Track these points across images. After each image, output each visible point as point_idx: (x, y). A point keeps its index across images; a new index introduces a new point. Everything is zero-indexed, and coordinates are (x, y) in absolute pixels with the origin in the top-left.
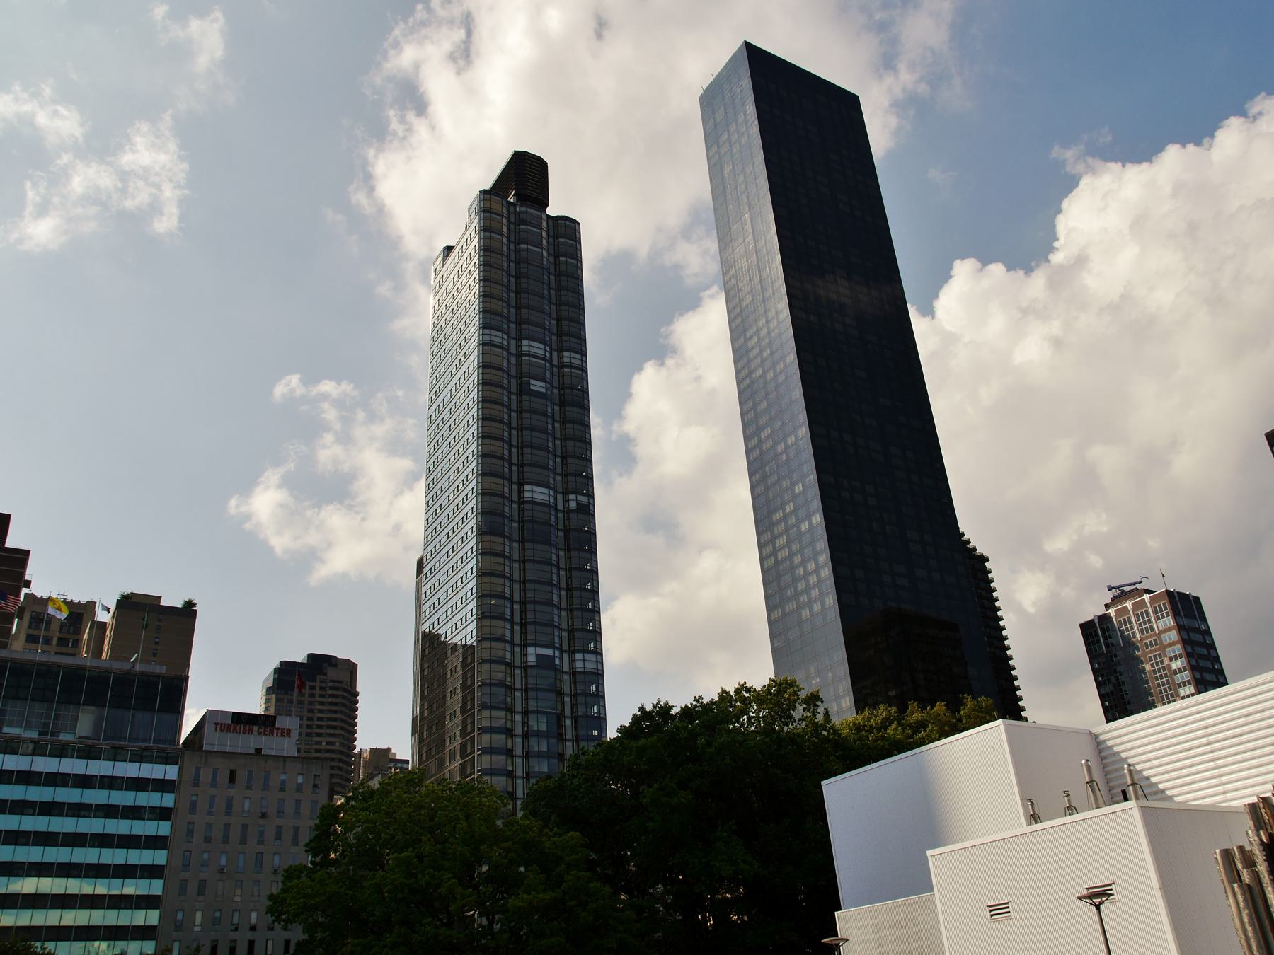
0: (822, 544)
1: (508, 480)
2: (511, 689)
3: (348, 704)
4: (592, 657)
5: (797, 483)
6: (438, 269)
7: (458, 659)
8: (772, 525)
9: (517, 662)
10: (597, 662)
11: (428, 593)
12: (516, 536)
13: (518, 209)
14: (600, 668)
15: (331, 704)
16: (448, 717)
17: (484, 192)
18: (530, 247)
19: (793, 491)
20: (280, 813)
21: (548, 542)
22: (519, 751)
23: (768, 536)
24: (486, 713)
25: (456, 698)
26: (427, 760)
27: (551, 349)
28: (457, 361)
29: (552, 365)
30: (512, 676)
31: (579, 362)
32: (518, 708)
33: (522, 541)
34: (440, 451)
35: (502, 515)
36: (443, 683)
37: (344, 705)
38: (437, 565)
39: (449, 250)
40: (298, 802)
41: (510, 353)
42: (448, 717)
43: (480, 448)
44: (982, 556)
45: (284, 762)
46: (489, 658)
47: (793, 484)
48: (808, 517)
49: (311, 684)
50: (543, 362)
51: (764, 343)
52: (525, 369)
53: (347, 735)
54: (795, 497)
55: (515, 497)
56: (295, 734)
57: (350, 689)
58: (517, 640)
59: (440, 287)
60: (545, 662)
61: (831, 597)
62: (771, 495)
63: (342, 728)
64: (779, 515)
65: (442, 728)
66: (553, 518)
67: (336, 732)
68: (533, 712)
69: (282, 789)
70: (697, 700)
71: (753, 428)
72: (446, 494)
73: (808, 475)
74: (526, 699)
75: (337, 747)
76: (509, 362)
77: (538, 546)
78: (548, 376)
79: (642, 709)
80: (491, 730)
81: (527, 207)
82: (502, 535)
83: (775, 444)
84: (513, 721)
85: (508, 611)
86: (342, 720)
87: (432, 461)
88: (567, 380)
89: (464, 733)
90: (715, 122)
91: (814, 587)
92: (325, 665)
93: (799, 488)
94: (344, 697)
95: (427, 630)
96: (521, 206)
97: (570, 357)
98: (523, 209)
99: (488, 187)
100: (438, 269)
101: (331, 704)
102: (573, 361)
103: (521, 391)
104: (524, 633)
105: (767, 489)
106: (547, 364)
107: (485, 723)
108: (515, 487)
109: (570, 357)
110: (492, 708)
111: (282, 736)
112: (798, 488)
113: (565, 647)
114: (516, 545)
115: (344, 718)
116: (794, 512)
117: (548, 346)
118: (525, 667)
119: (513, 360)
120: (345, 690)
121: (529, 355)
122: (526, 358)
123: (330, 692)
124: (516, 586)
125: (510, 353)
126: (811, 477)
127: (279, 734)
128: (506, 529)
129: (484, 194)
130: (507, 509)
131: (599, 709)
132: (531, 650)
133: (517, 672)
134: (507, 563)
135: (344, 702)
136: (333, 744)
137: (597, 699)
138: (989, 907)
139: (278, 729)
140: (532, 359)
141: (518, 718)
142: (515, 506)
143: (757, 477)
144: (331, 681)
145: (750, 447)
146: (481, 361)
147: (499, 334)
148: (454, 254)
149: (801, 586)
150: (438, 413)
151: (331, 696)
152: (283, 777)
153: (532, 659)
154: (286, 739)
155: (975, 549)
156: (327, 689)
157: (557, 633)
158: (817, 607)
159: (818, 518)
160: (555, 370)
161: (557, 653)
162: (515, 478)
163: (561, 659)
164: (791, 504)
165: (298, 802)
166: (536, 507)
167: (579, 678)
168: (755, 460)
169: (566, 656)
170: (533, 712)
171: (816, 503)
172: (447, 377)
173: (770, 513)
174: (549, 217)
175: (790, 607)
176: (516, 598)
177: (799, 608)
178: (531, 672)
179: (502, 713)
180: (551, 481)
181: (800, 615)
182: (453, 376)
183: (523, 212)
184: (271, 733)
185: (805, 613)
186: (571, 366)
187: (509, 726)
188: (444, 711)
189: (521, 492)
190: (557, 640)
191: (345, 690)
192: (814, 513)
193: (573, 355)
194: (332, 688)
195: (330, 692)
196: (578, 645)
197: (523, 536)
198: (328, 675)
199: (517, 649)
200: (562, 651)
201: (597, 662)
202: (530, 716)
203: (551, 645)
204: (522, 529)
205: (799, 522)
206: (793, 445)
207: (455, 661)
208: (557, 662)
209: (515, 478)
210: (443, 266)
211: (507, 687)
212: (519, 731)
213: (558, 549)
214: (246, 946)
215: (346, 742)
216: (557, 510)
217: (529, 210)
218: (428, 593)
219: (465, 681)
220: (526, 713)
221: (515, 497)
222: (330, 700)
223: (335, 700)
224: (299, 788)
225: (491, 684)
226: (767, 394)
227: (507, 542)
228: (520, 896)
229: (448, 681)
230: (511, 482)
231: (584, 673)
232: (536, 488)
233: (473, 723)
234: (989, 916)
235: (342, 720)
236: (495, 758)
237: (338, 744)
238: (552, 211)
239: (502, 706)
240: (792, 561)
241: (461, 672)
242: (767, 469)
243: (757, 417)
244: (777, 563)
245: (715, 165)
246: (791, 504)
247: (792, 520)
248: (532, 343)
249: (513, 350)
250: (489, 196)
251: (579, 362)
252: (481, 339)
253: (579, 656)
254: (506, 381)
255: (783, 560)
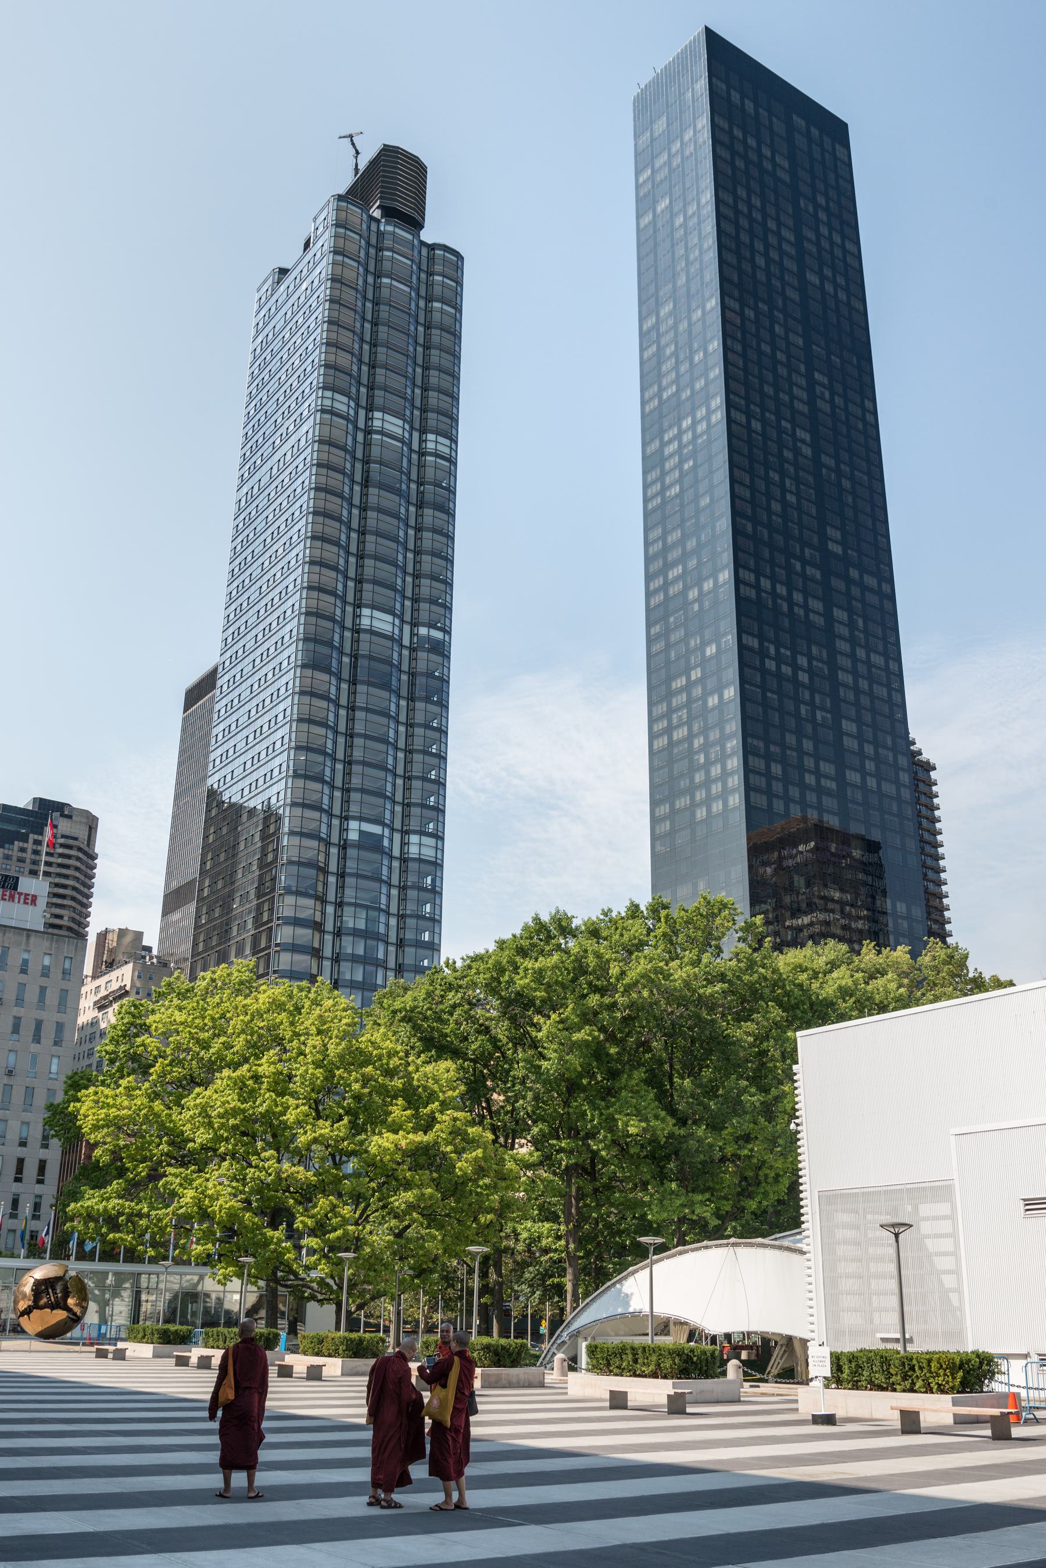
0: (734, 726)
1: (340, 597)
2: (325, 871)
3: (83, 867)
4: (431, 841)
5: (709, 643)
6: (263, 299)
7: (257, 826)
8: (670, 694)
9: (335, 839)
10: (437, 848)
11: (220, 736)
12: (345, 675)
13: (382, 228)
14: (439, 856)
15: (60, 865)
16: (237, 900)
17: (340, 198)
18: (395, 283)
19: (703, 653)
20: (20, 1001)
21: (386, 686)
22: (328, 952)
23: (662, 708)
24: (290, 900)
25: (250, 877)
26: (205, 951)
27: (412, 428)
28: (283, 430)
29: (411, 450)
30: (327, 855)
31: (447, 450)
32: (331, 896)
33: (353, 682)
34: (250, 550)
35: (330, 644)
36: (233, 856)
37: (77, 869)
38: (236, 701)
39: (283, 272)
40: (43, 990)
41: (356, 428)
42: (237, 900)
43: (308, 551)
44: (928, 763)
45: (28, 936)
46: (299, 830)
47: (704, 644)
48: (719, 690)
49: (36, 837)
50: (400, 445)
51: (685, 451)
52: (375, 451)
53: (78, 907)
54: (704, 662)
55: (348, 623)
56: (42, 902)
57: (86, 849)
58: (337, 811)
59: (265, 325)
60: (370, 844)
61: (737, 796)
62: (673, 654)
63: (73, 899)
64: (680, 682)
65: (228, 914)
66: (396, 656)
67: (65, 902)
68: (350, 904)
69: (24, 971)
70: (605, 914)
71: (658, 564)
72: (256, 609)
73: (725, 634)
74: (341, 887)
75: (65, 922)
76: (355, 439)
77: (373, 690)
78: (405, 464)
79: (537, 919)
80: (296, 922)
81: (395, 226)
82: (328, 670)
83: (686, 589)
84: (323, 913)
85: (328, 772)
86: (74, 889)
87: (237, 561)
88: (430, 473)
89: (258, 922)
90: (651, 135)
91: (716, 780)
92: (56, 814)
93: (711, 650)
94: (78, 859)
95: (215, 786)
96: (387, 223)
97: (436, 442)
98: (390, 228)
99: (342, 190)
100: (263, 299)
101: (60, 865)
102: (440, 447)
103: (367, 481)
104: (346, 802)
105: (668, 646)
106: (405, 448)
107: (288, 912)
108: (349, 609)
109: (436, 442)
110: (298, 893)
111: (25, 903)
112: (711, 650)
113: (397, 825)
114: (344, 686)
115: (77, 885)
116: (700, 681)
117: (408, 423)
118: (344, 846)
119: (360, 437)
120: (80, 849)
121: (382, 433)
122: (379, 437)
123: (60, 850)
124: (341, 740)
125: (356, 428)
126: (730, 637)
127: (22, 901)
128: (334, 663)
129: (339, 200)
130: (337, 637)
131: (433, 908)
132: (353, 825)
133: (334, 851)
134: (332, 708)
135: (78, 864)
136: (60, 917)
137: (432, 896)
138: (1024, 1200)
139: (20, 894)
140: (385, 438)
141: (330, 909)
142: (348, 634)
143: (656, 629)
144: (63, 836)
145: (652, 588)
146: (317, 434)
147: (345, 399)
148: (289, 280)
149: (699, 777)
150: (251, 498)
151: (61, 855)
152: (26, 956)
153: (353, 836)
154: (31, 908)
155: (920, 753)
156: (57, 846)
157: (388, 806)
158: (717, 807)
159: (731, 693)
160: (415, 456)
161: (387, 832)
162: (350, 598)
163: (391, 840)
164: (699, 670)
165: (43, 990)
166: (375, 639)
167: (412, 866)
168: (657, 606)
169: (397, 837)
170: (350, 904)
171: (732, 672)
172: (267, 449)
173: (670, 679)
174: (423, 243)
175: (682, 803)
176: (340, 755)
177: (694, 806)
178: (352, 852)
179: (310, 902)
180: (398, 606)
181: (693, 814)
182: (275, 450)
183: (389, 233)
184: (12, 898)
185: (701, 813)
186: (437, 455)
187: (318, 919)
188: (233, 891)
189: (356, 616)
190: (388, 815)
191: (80, 849)
192: (727, 686)
193: (440, 439)
194: (62, 846)
195: (60, 850)
196: (414, 824)
197: (355, 675)
198: (59, 827)
199: (336, 822)
200: (393, 830)
201: (437, 848)
202: (346, 908)
203: (378, 821)
204: (354, 666)
205: (706, 695)
206: (709, 592)
207: (251, 831)
208: (386, 843)
209: (350, 598)
210: (272, 295)
211: (319, 869)
212: (329, 926)
213: (399, 696)
214: (15, 1163)
215: (77, 917)
216: (401, 646)
217: (397, 231)
218: (220, 736)
219: (264, 855)
220: (339, 905)
221: (348, 623)
222: (60, 860)
223: (66, 861)
224: (46, 972)
225: (299, 864)
226: (683, 520)
227: (334, 681)
228: (385, 1135)
229: (241, 855)
230: (345, 602)
231: (420, 860)
232: (377, 614)
233: (271, 910)
234: (1023, 1211)
235: (74, 889)
236: (298, 957)
237: (66, 918)
238: (428, 235)
239: (311, 892)
240: (691, 744)
241: (259, 844)
242: (672, 619)
243: (666, 549)
244: (671, 744)
245: (645, 196)
246: (699, 670)
247: (697, 691)
248: (387, 417)
249: (361, 424)
250: (345, 204)
251: (447, 450)
252: (319, 403)
253: (414, 839)
254: (348, 466)
255: (680, 742)
